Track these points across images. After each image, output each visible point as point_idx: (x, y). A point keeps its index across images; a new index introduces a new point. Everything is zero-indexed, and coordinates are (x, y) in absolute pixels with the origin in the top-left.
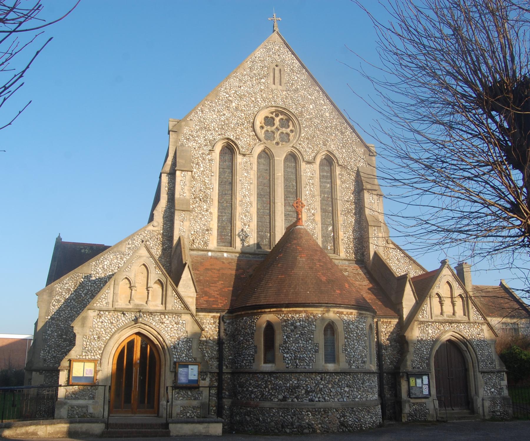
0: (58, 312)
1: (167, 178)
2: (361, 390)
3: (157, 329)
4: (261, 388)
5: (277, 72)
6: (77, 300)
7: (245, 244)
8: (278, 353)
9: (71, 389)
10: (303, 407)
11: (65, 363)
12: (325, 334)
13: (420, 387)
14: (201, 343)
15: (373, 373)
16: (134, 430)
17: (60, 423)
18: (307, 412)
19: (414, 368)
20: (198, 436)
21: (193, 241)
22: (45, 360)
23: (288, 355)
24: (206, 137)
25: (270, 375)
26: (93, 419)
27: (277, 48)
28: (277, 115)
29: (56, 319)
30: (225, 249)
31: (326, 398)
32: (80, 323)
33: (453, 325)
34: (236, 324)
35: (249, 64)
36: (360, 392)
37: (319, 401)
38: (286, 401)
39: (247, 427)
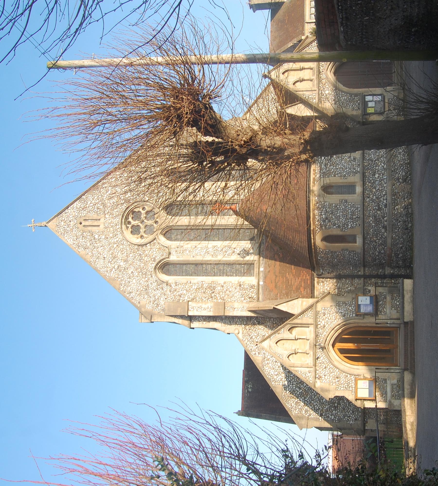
0: (316, 410)
1: (194, 322)
3: (330, 331)
4: (376, 245)
5: (87, 223)
6: (305, 396)
7: (251, 252)
8: (348, 232)
9: (378, 398)
10: (391, 213)
11: (358, 404)
12: (332, 193)
13: (375, 104)
14: (339, 295)
15: (363, 153)
16: (409, 349)
17: (404, 405)
18: (395, 209)
20: (413, 298)
21: (250, 298)
22: (356, 419)
23: (350, 224)
24: (155, 288)
25: (366, 238)
26: (401, 380)
27: (63, 223)
28: (129, 223)
29: (322, 412)
30: (256, 270)
31: (384, 193)
32: (326, 393)
33: (321, 70)
34: (323, 264)
35: (81, 250)
36: (379, 164)
37: (386, 199)
38: (386, 226)
39: (408, 256)
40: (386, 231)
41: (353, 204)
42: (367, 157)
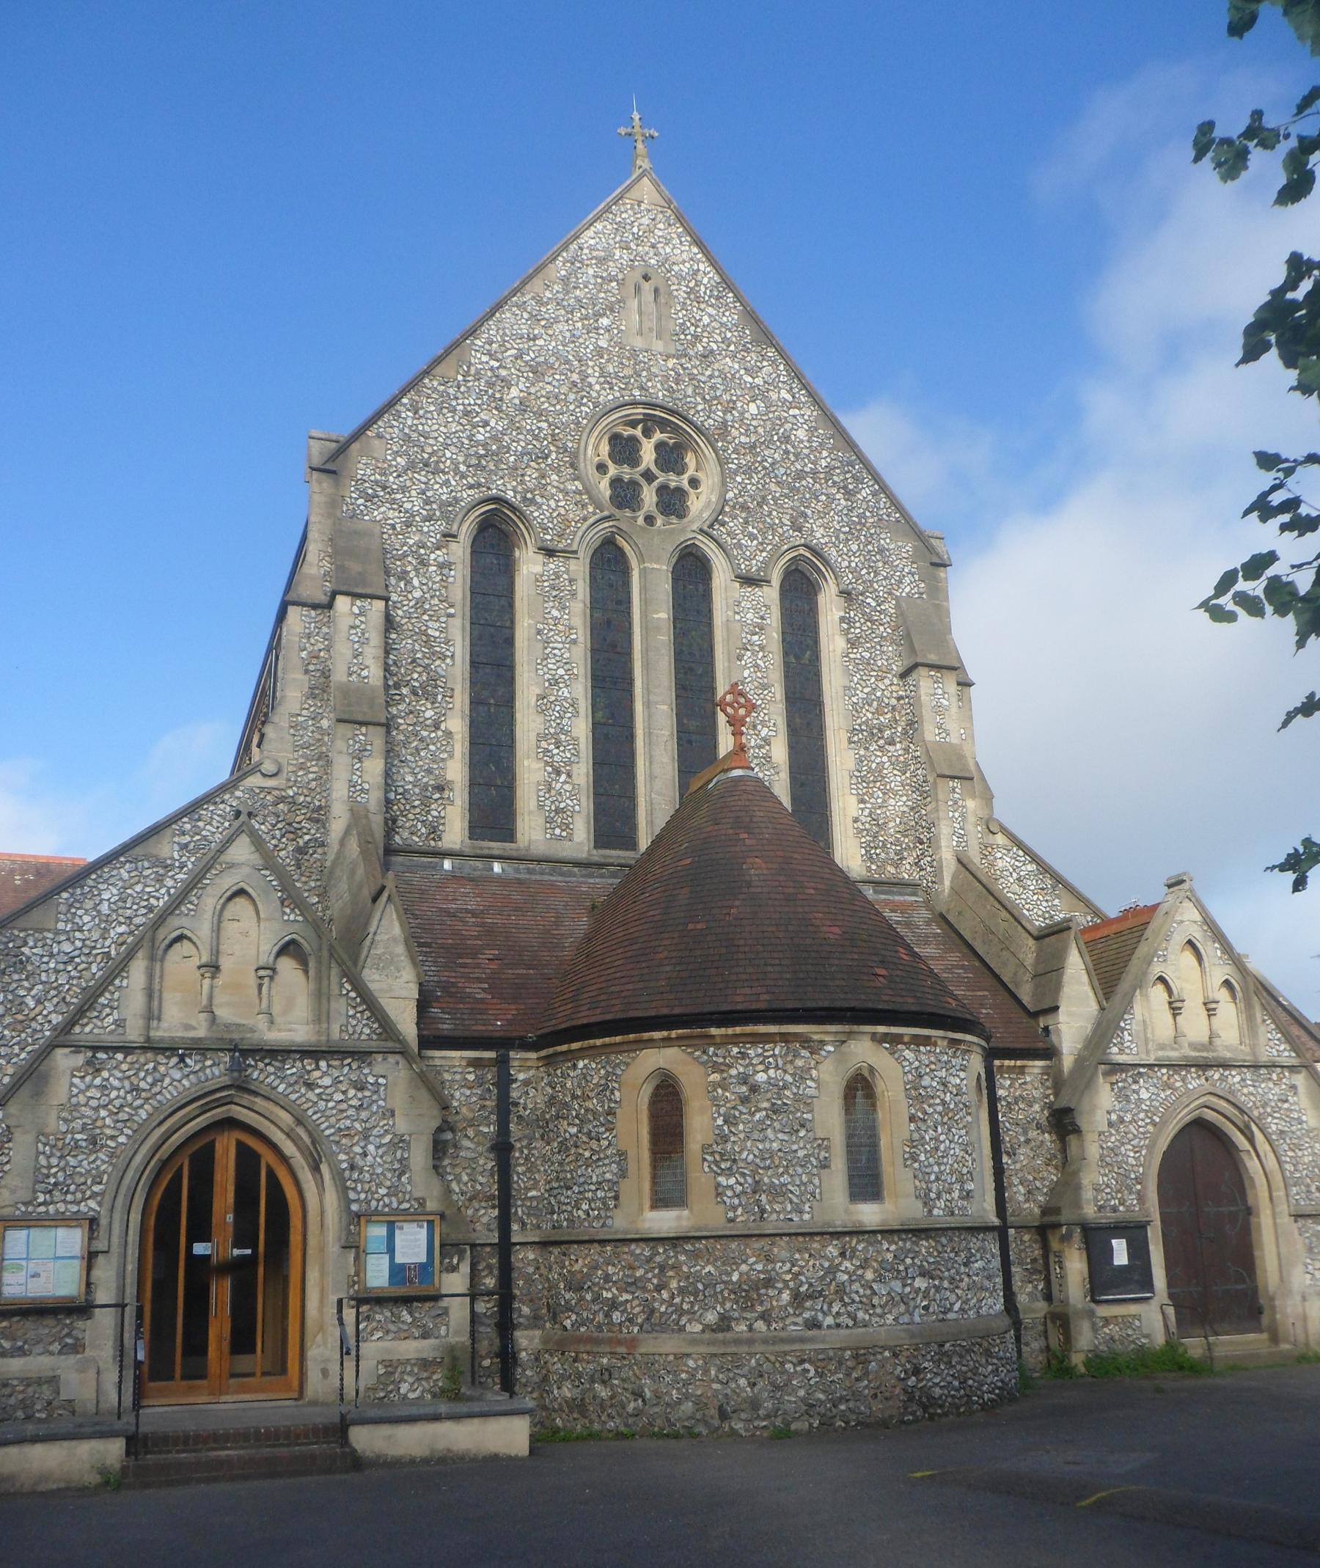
2: (963, 1285)
4: (644, 1289)
5: (648, 296)
8: (699, 1174)
18: (802, 1362)
19: (1100, 1208)
23: (732, 1181)
24: (429, 494)
25: (675, 1246)
28: (647, 433)
31: (860, 1315)
33: (1210, 1073)
35: (560, 268)
40: (707, 1328)
41: (813, 1195)
42: (975, 1243)
